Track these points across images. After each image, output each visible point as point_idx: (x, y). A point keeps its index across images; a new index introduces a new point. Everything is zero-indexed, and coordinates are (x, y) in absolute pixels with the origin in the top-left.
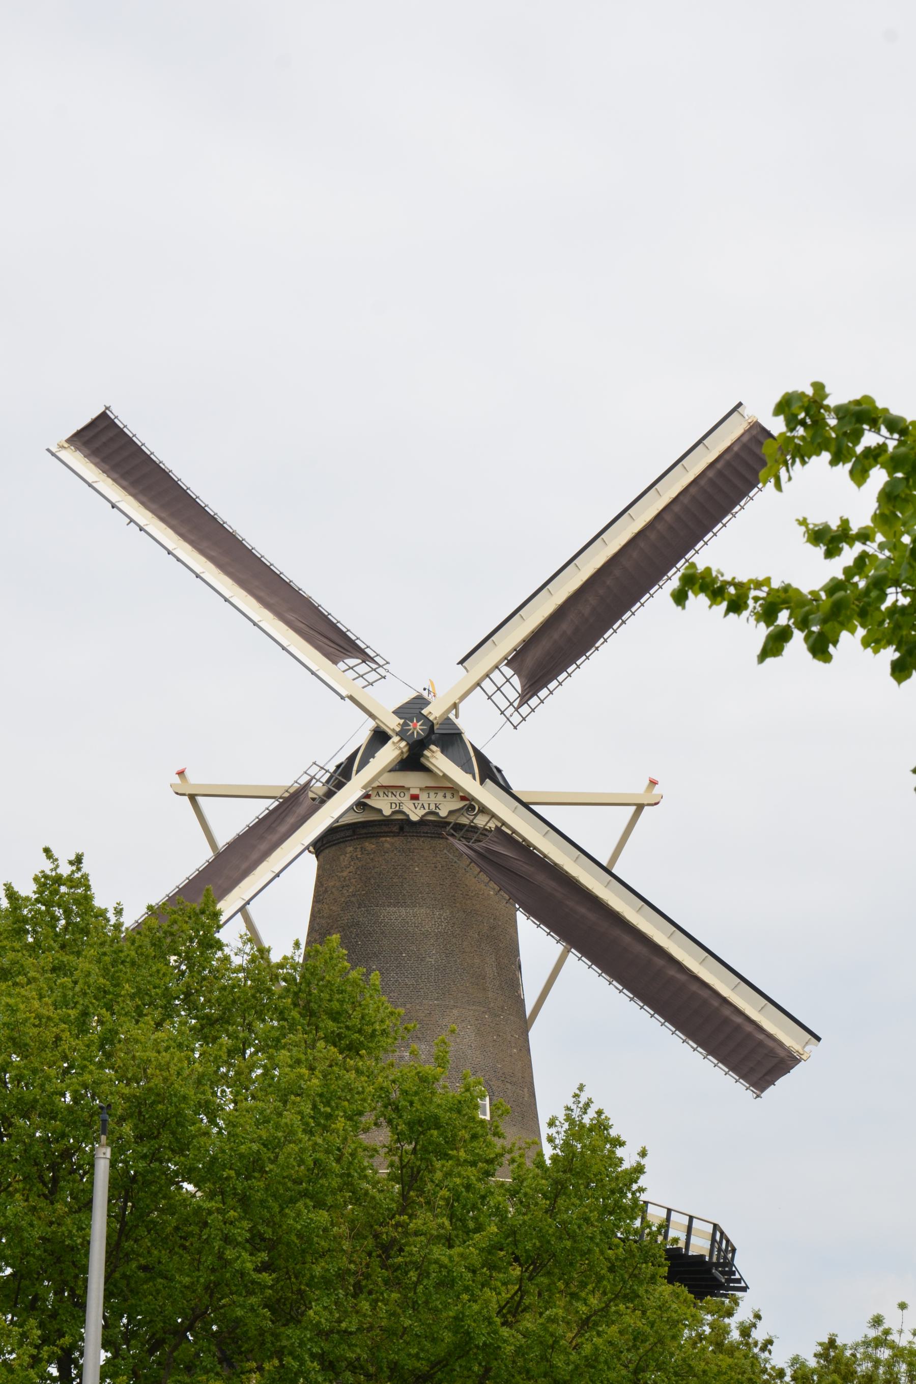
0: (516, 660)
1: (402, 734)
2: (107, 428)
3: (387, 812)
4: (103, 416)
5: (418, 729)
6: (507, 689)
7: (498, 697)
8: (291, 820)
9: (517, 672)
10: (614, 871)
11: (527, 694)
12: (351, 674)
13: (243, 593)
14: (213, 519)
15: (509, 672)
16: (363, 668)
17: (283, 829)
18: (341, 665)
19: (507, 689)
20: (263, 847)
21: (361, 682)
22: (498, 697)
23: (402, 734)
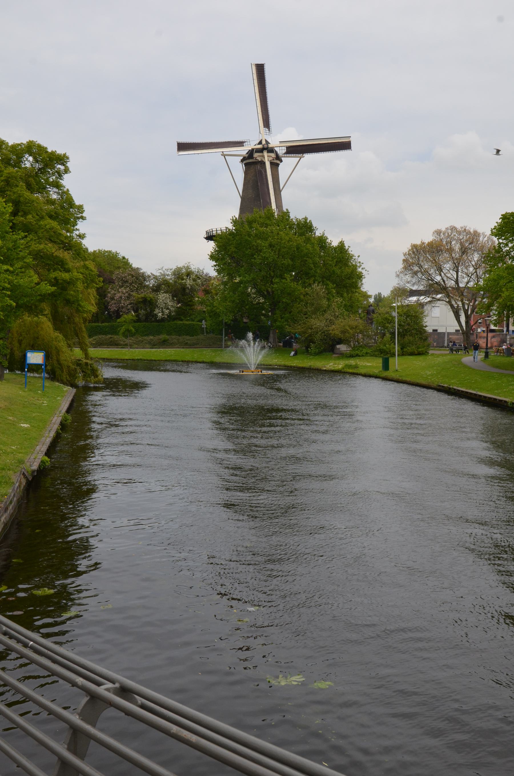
0: (288, 148)
1: (263, 145)
2: (262, 69)
3: (260, 160)
4: (263, 64)
5: (266, 146)
6: (283, 151)
7: (281, 151)
8: (239, 145)
9: (287, 149)
10: (479, 410)
11: (245, 142)
12: (265, 131)
13: (209, 150)
14: (266, 92)
15: (285, 148)
16: (268, 131)
17: (237, 145)
18: (265, 129)
19: (283, 151)
20: (232, 145)
21: (265, 133)
22: (281, 151)
23: (263, 145)
